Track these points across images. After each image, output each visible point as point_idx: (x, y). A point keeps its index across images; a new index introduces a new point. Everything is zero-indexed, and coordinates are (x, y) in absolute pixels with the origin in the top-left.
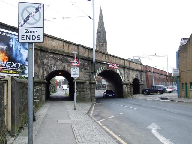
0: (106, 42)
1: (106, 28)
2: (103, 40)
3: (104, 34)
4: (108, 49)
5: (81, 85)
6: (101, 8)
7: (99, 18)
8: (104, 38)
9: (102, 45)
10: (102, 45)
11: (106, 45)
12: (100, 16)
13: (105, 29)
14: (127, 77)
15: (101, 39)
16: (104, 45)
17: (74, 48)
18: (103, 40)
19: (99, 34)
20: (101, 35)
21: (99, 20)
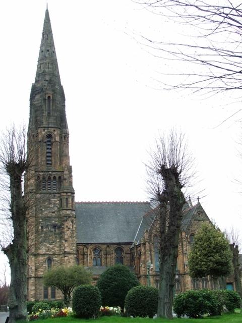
0: (66, 127)
1: (64, 81)
2: (52, 120)
3: (58, 97)
4: (71, 154)
5: (74, 248)
6: (47, 100)
7: (41, 46)
8: (55, 111)
9: (49, 136)
10: (49, 136)
11: (65, 137)
12: (43, 40)
13: (62, 83)
14: (174, 267)
15: (46, 114)
16: (57, 139)
17: (31, 246)
18: (52, 120)
19: (37, 97)
20: (45, 99)
21: (42, 51)
